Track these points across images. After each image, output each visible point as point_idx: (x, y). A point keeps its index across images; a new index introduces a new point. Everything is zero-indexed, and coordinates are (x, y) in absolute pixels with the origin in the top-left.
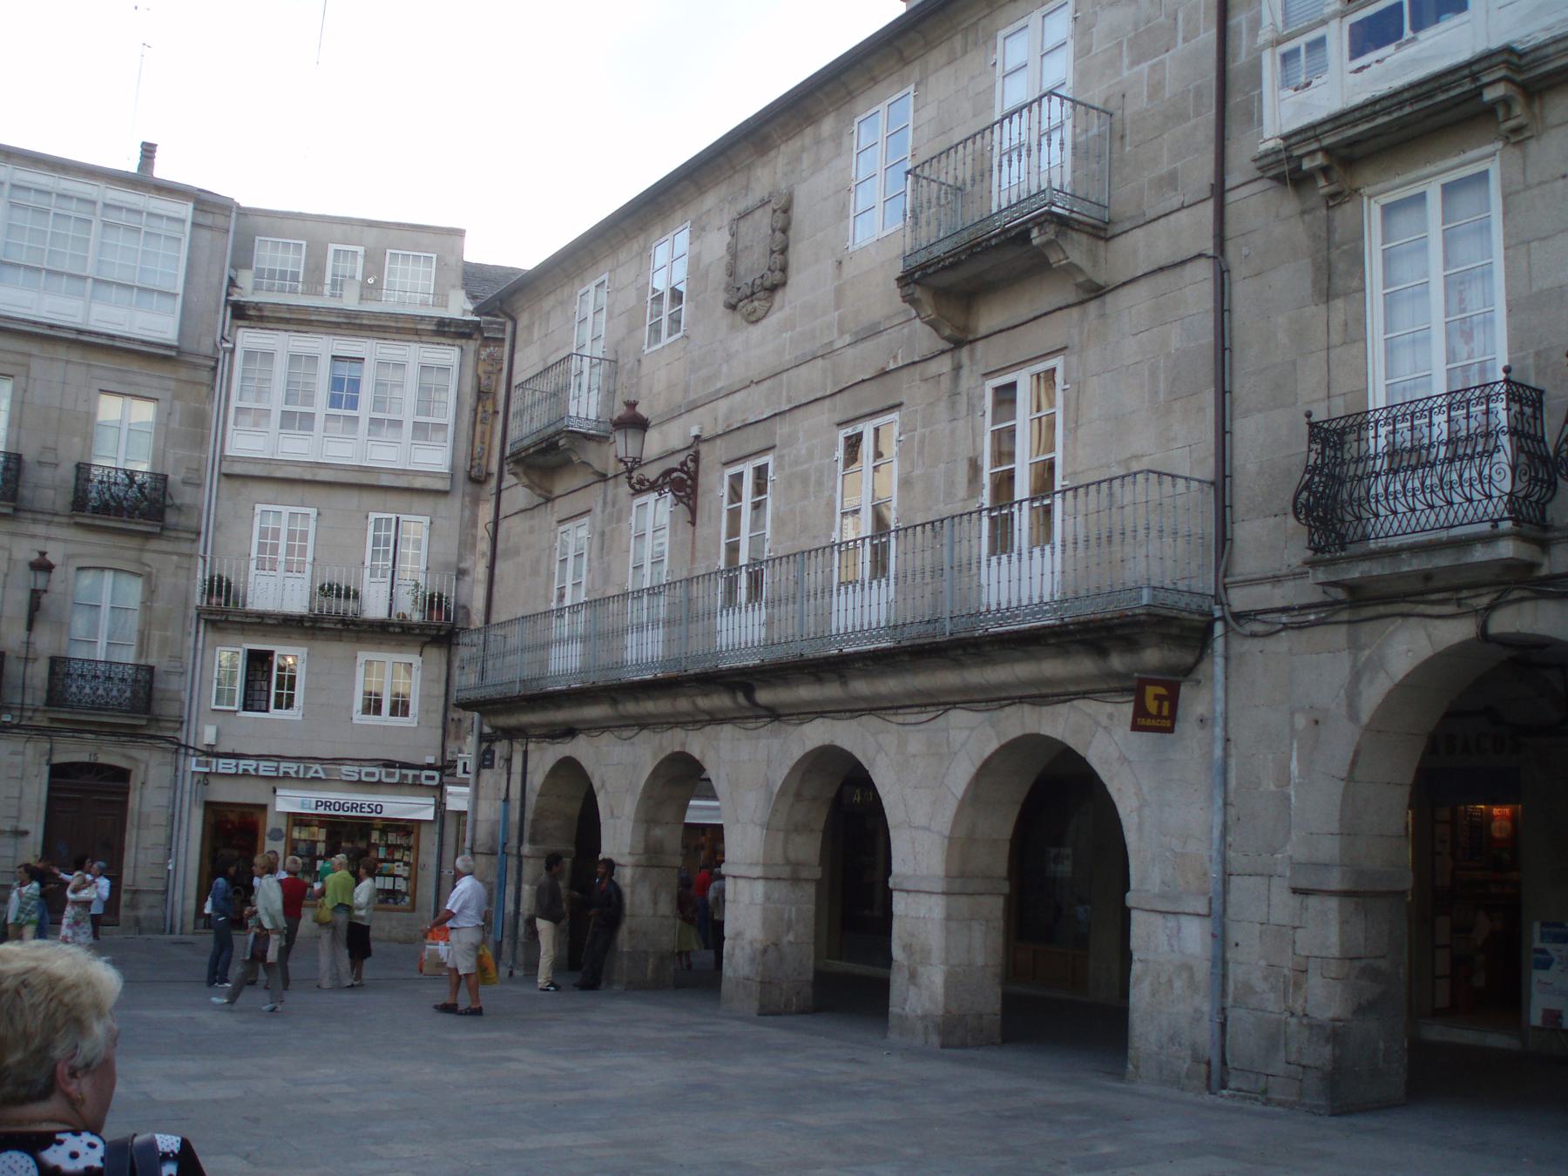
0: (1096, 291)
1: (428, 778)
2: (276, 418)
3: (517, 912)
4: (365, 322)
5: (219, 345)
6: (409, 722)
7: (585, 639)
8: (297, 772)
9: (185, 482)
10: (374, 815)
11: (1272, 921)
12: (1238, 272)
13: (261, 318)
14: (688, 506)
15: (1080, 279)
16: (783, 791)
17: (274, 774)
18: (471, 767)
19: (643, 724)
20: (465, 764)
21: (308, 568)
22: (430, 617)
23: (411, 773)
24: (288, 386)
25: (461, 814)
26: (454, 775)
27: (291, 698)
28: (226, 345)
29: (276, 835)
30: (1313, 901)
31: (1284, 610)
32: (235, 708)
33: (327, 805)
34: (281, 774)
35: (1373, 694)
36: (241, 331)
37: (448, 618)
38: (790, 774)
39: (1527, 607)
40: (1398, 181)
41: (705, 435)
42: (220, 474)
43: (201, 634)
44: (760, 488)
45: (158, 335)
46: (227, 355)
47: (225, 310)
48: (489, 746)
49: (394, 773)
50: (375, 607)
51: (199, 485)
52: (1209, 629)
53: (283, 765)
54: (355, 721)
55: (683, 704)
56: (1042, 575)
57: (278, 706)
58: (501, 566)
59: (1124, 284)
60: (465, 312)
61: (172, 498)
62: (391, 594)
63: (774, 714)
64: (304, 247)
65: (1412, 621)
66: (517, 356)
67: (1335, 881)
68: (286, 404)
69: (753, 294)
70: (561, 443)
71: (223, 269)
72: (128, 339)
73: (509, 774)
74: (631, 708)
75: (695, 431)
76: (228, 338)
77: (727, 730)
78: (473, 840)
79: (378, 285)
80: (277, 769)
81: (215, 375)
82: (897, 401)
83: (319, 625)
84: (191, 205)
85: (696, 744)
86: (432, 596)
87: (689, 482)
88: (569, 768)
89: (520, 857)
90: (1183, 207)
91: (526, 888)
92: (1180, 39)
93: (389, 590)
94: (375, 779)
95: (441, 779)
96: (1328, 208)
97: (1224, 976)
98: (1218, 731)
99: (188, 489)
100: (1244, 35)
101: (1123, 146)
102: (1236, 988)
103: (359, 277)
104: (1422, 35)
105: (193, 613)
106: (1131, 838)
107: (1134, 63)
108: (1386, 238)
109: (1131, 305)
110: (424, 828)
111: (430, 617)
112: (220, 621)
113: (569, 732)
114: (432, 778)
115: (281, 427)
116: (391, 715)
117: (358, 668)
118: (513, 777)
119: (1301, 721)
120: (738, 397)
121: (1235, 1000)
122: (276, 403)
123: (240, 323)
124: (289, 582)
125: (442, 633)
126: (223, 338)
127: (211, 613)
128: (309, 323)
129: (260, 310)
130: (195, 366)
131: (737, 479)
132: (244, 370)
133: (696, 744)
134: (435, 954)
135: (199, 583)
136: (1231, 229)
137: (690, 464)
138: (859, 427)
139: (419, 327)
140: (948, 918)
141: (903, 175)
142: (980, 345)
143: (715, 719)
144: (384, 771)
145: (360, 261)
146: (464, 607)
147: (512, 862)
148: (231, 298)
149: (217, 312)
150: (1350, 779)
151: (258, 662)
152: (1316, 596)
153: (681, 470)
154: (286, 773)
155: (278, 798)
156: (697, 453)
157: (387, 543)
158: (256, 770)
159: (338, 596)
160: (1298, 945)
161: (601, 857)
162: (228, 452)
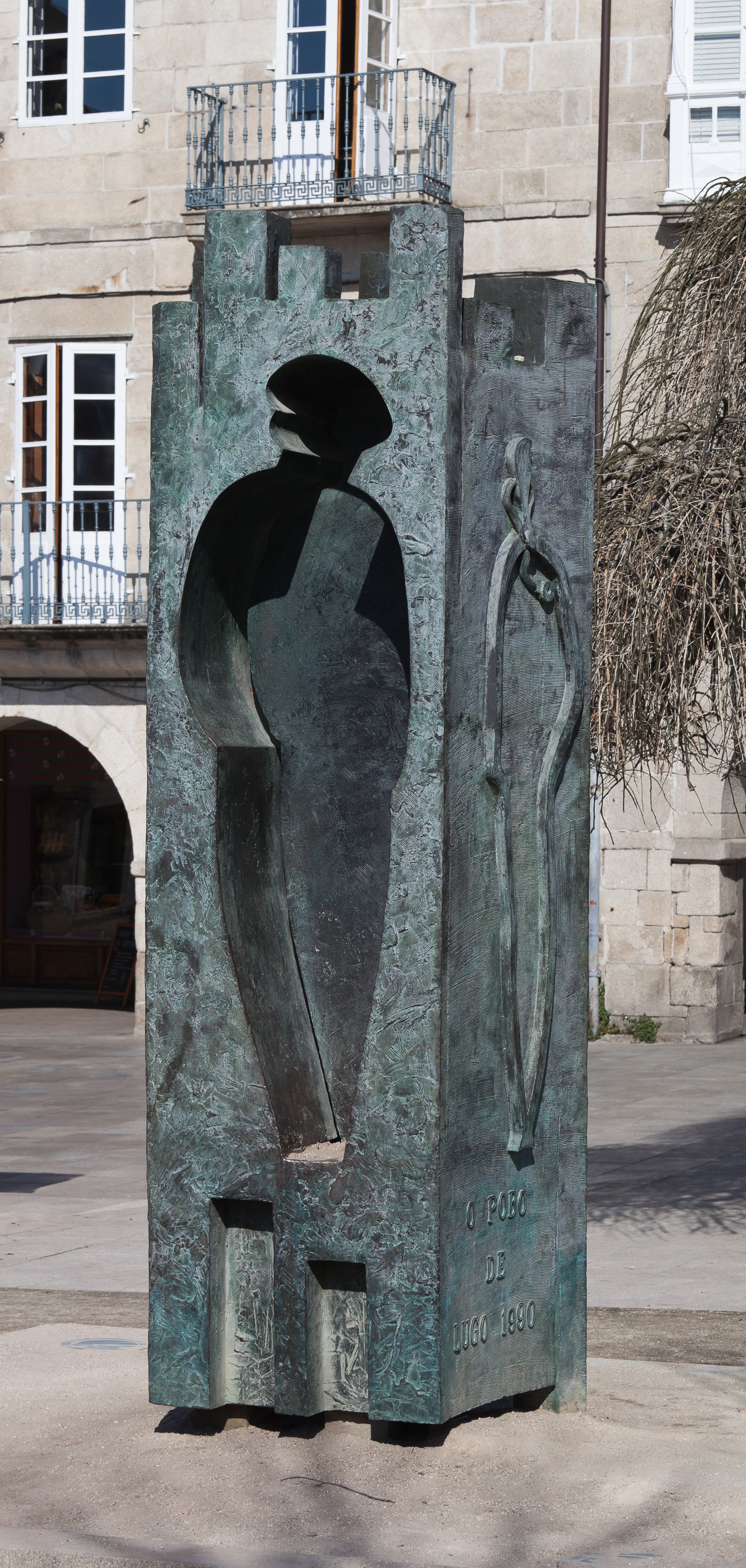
11: (649, 887)
56: (139, 528)
90: (554, 216)
100: (630, 57)
101: (470, 126)
102: (611, 947)
121: (611, 957)
141: (186, 91)
160: (679, 907)
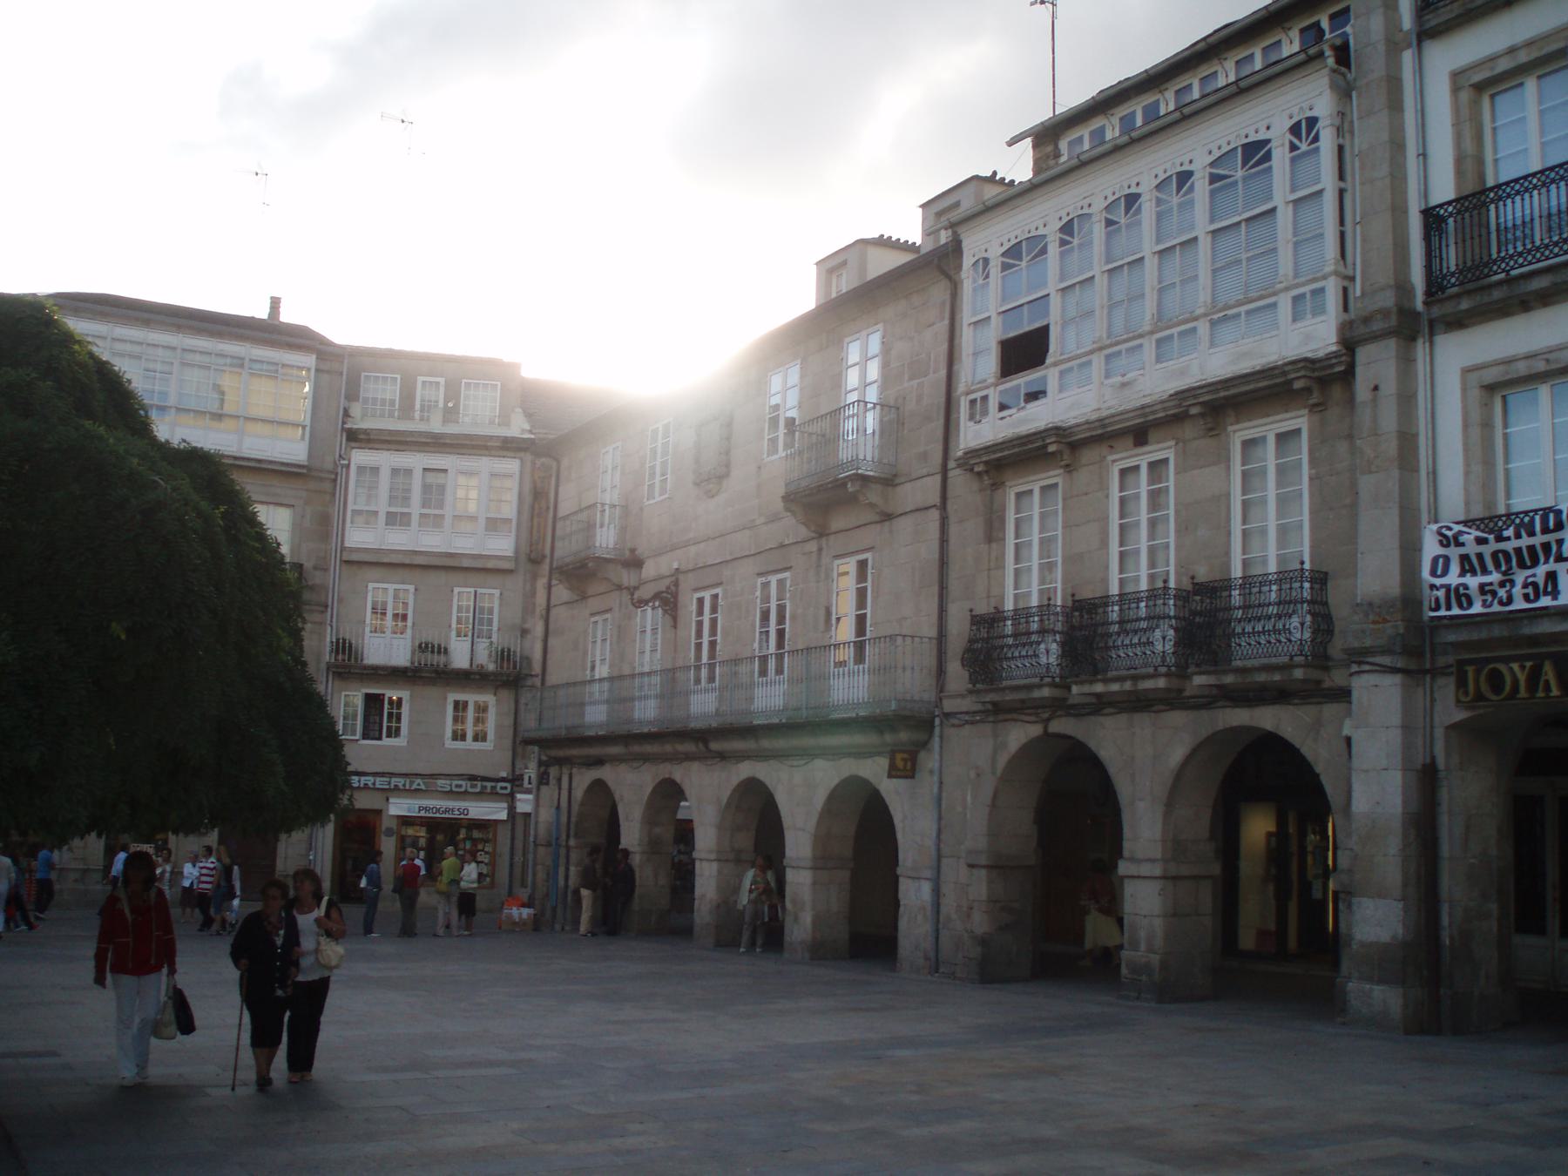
0: (888, 517)
1: (502, 788)
2: (382, 517)
3: (566, 886)
4: (448, 441)
5: (338, 462)
6: (488, 745)
7: (608, 702)
8: (404, 785)
9: (315, 568)
10: (462, 816)
12: (952, 519)
13: (369, 441)
14: (670, 615)
15: (878, 510)
16: (728, 804)
17: (388, 787)
18: (534, 781)
19: (646, 758)
20: (530, 777)
21: (409, 631)
22: (502, 667)
23: (489, 785)
24: (391, 492)
25: (527, 815)
26: (522, 785)
27: (398, 730)
28: (342, 462)
29: (389, 832)
30: (975, 871)
31: (967, 713)
32: (357, 738)
33: (426, 809)
34: (392, 787)
35: (1003, 760)
36: (354, 450)
37: (515, 667)
38: (732, 794)
39: (1063, 720)
40: (1021, 481)
41: (683, 568)
42: (341, 560)
43: (330, 682)
44: (714, 609)
45: (286, 456)
46: (344, 470)
47: (342, 436)
48: (546, 770)
49: (476, 785)
50: (460, 658)
51: (326, 570)
52: (932, 722)
53: (393, 780)
54: (446, 746)
55: (668, 748)
57: (389, 736)
58: (552, 642)
59: (901, 515)
60: (523, 431)
61: (306, 580)
62: (472, 650)
63: (722, 757)
64: (399, 381)
65: (1020, 723)
66: (561, 489)
67: (983, 860)
68: (390, 506)
69: (710, 479)
70: (590, 565)
71: (339, 402)
72: (271, 462)
73: (560, 789)
74: (636, 748)
75: (675, 566)
76: (344, 456)
77: (695, 766)
78: (536, 836)
79: (456, 409)
80: (389, 783)
81: (335, 486)
82: (789, 566)
83: (418, 674)
84: (314, 357)
85: (677, 773)
86: (503, 651)
87: (672, 600)
88: (599, 786)
89: (568, 848)
91: (572, 869)
92: (931, 372)
93: (470, 646)
94: (463, 790)
95: (512, 789)
96: (992, 491)
97: (938, 912)
98: (936, 778)
99: (318, 573)
103: (441, 405)
104: (1030, 406)
105: (323, 666)
106: (899, 836)
107: (911, 379)
108: (1018, 511)
109: (904, 525)
110: (500, 827)
111: (502, 667)
112: (345, 673)
113: (599, 762)
114: (506, 788)
115: (386, 525)
116: (467, 702)
117: (448, 706)
118: (562, 792)
119: (972, 774)
120: (702, 546)
122: (382, 506)
123: (353, 444)
124: (395, 642)
125: (511, 679)
126: (340, 456)
127: (337, 667)
128: (406, 443)
129: (368, 434)
130: (322, 480)
131: (701, 601)
132: (357, 481)
133: (677, 773)
134: (510, 916)
135: (328, 644)
136: (950, 494)
137: (673, 588)
138: (769, 578)
139: (489, 444)
140: (814, 883)
142: (832, 537)
143: (689, 757)
144: (469, 783)
145: (442, 390)
146: (527, 658)
147: (563, 851)
148: (346, 426)
149: (336, 436)
150: (993, 805)
151: (373, 702)
152: (979, 707)
153: (668, 593)
154: (396, 786)
155: (390, 805)
156: (677, 580)
157: (468, 611)
158: (374, 784)
159: (433, 652)
161: (620, 847)
162: (347, 545)
